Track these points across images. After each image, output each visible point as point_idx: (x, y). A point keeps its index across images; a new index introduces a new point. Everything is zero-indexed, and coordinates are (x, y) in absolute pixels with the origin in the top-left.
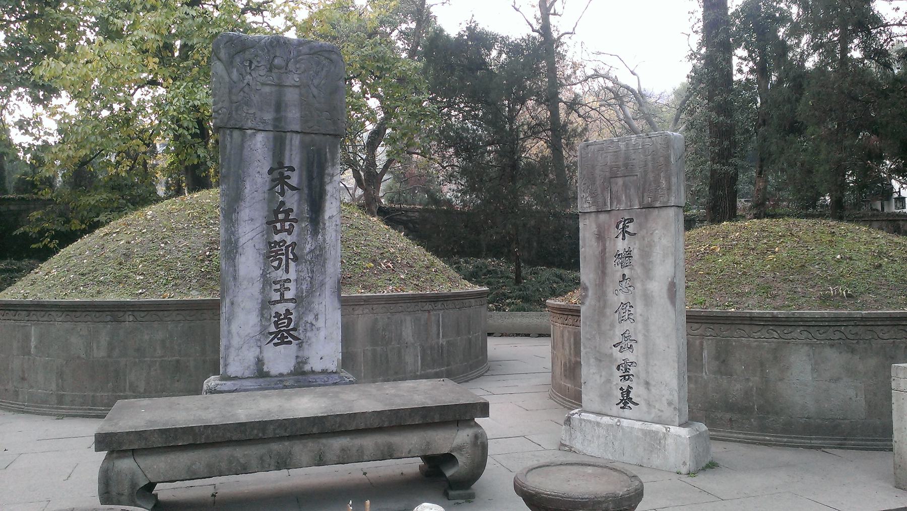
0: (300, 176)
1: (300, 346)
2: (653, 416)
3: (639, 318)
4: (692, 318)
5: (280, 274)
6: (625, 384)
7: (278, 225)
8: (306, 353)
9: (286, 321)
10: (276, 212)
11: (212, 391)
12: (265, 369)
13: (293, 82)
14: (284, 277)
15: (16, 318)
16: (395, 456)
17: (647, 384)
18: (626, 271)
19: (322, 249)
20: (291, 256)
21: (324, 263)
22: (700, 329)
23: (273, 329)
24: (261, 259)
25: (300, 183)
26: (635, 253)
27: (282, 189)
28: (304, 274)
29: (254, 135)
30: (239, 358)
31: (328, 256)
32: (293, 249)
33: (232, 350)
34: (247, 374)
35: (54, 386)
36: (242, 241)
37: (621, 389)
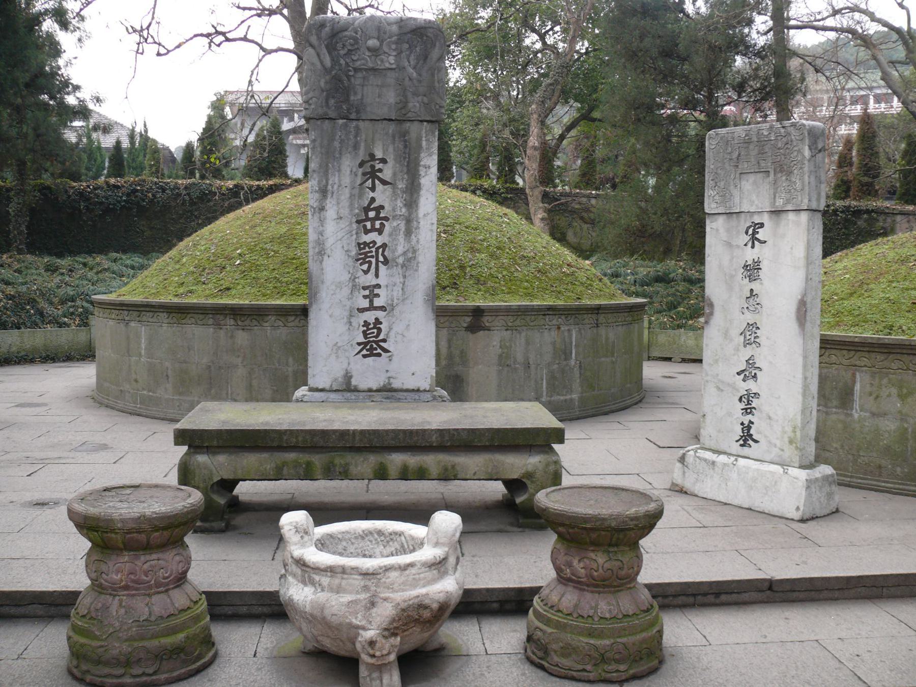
2: (773, 455)
4: (827, 344)
6: (746, 419)
9: (375, 331)
10: (367, 210)
11: (300, 401)
13: (387, 65)
14: (374, 282)
16: (459, 477)
19: (414, 251)
20: (381, 259)
21: (418, 266)
22: (835, 356)
26: (764, 265)
28: (398, 280)
30: (323, 368)
31: (420, 258)
32: (383, 251)
37: (742, 424)
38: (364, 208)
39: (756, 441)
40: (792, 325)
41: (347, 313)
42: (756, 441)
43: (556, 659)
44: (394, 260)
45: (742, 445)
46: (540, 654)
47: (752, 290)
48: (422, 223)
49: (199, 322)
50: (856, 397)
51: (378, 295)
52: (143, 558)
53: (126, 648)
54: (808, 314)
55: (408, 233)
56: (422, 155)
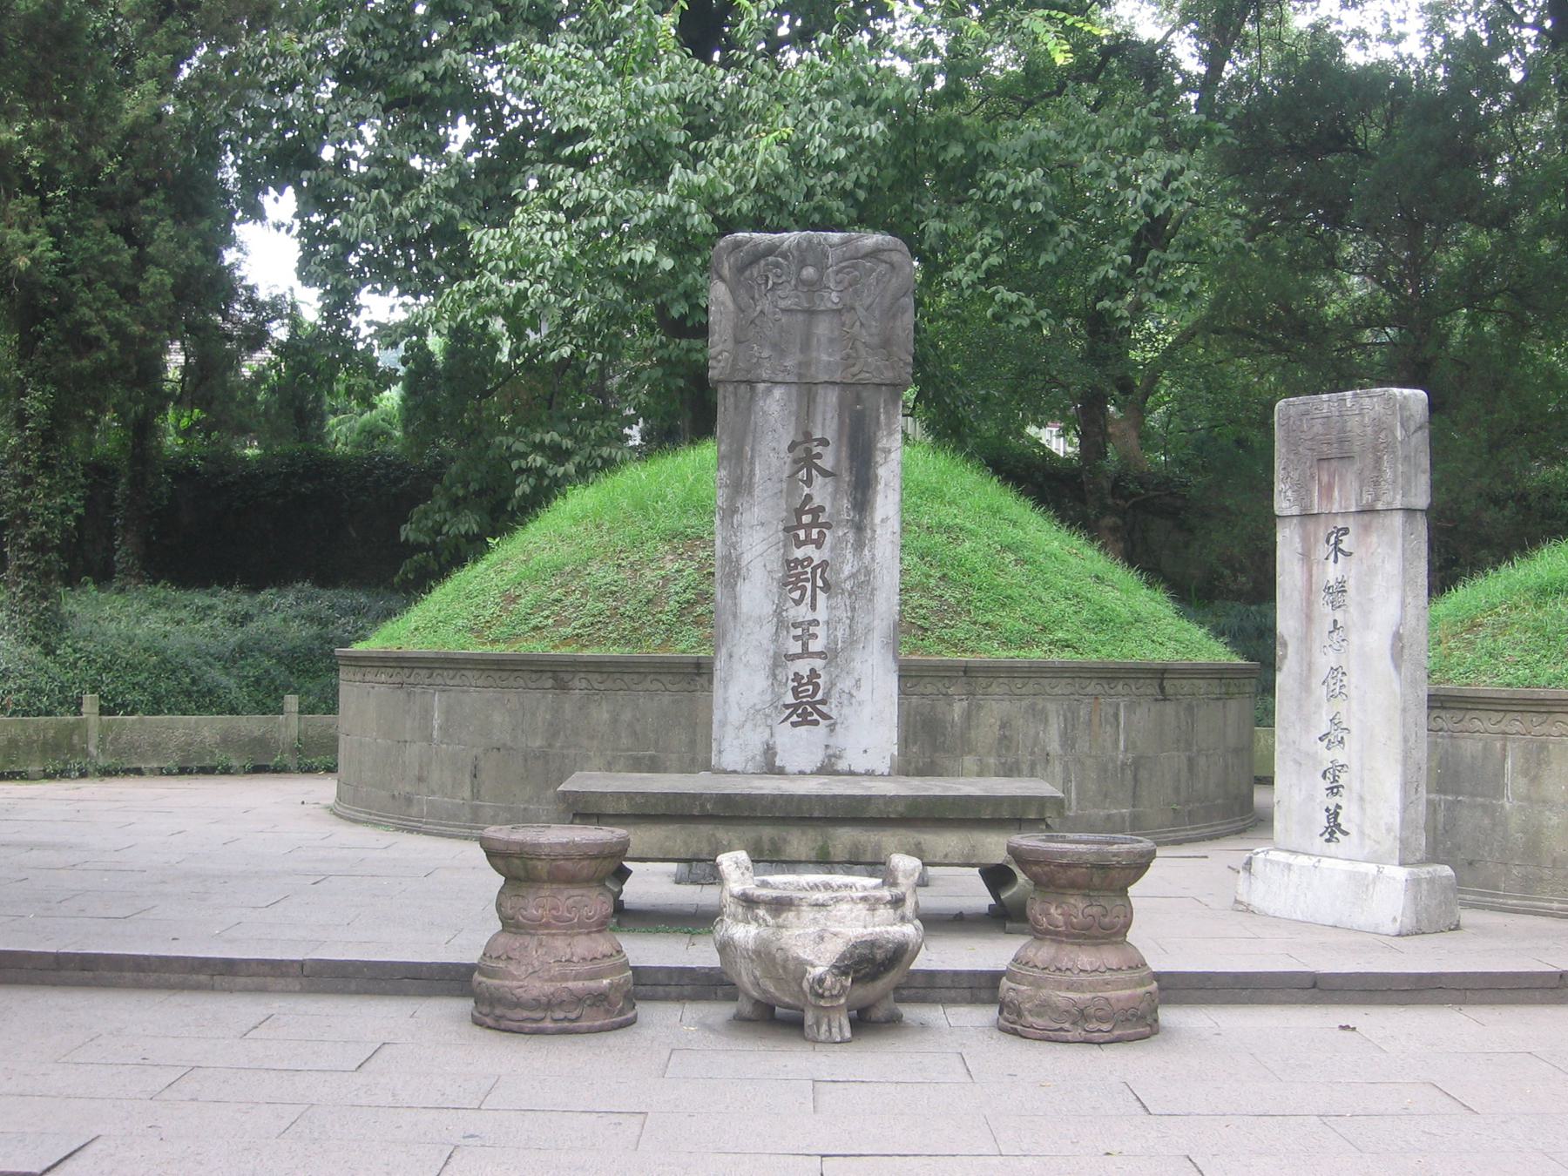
0: (838, 451)
1: (832, 728)
2: (1367, 850)
3: (1353, 693)
5: (802, 612)
6: (1331, 802)
7: (802, 534)
8: (841, 739)
10: (799, 512)
12: (778, 763)
13: (829, 305)
14: (809, 617)
15: (412, 680)
17: (1361, 799)
18: (1339, 615)
19: (868, 573)
20: (820, 583)
21: (872, 594)
23: (790, 699)
24: (775, 588)
25: (838, 461)
26: (1351, 586)
27: (809, 474)
28: (843, 614)
29: (769, 391)
31: (878, 583)
33: (730, 730)
34: (750, 768)
35: (467, 794)
36: (746, 558)
38: (796, 510)
39: (1345, 833)
40: (1385, 664)
41: (770, 662)
42: (1345, 833)
43: (1030, 1019)
44: (838, 585)
45: (1328, 841)
46: (1013, 1017)
47: (1335, 622)
48: (878, 531)
49: (531, 685)
50: (1508, 779)
51: (814, 636)
52: (566, 893)
53: (549, 988)
54: (1406, 651)
55: (859, 546)
56: (880, 434)
